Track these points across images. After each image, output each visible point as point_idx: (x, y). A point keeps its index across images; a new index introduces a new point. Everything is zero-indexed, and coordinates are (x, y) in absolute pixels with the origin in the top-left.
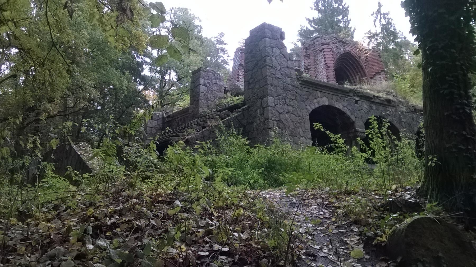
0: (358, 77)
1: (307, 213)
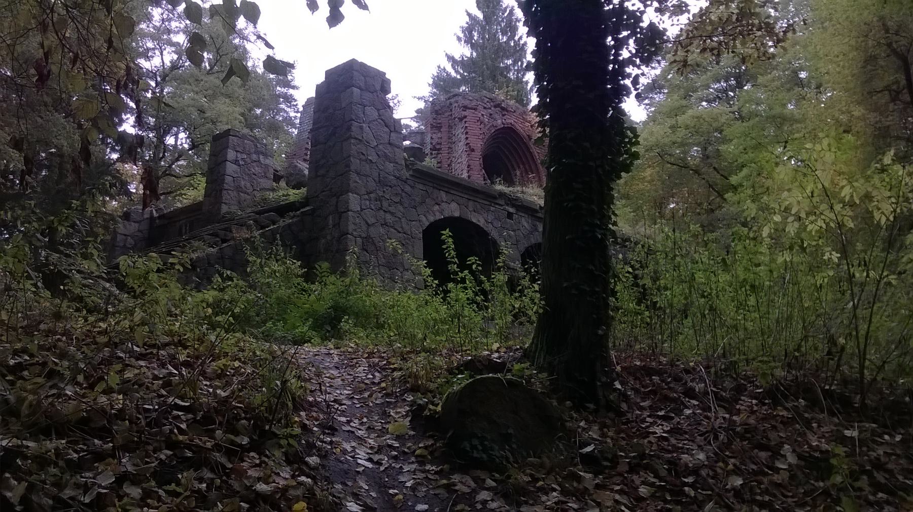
0: (518, 173)
1: (349, 377)
